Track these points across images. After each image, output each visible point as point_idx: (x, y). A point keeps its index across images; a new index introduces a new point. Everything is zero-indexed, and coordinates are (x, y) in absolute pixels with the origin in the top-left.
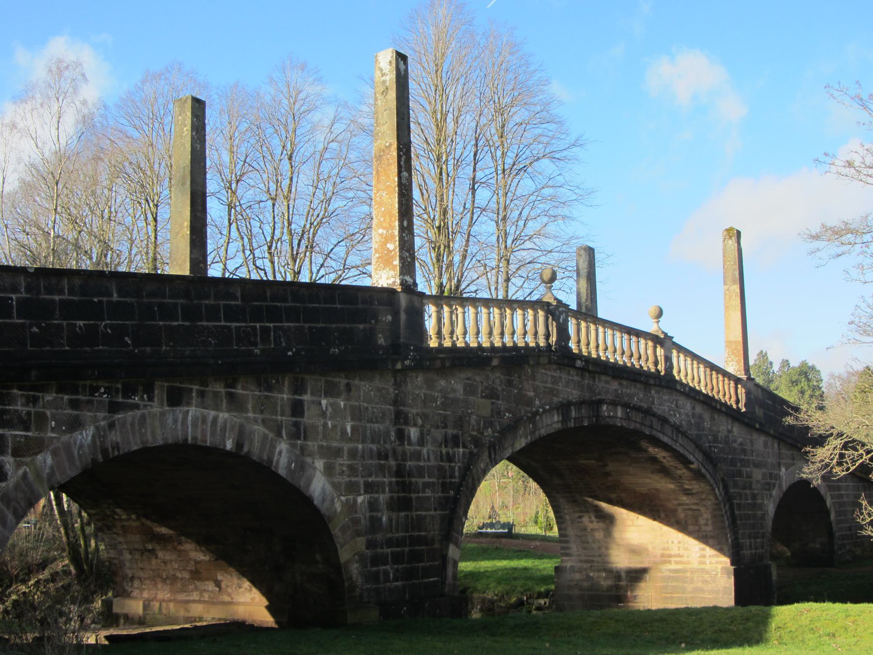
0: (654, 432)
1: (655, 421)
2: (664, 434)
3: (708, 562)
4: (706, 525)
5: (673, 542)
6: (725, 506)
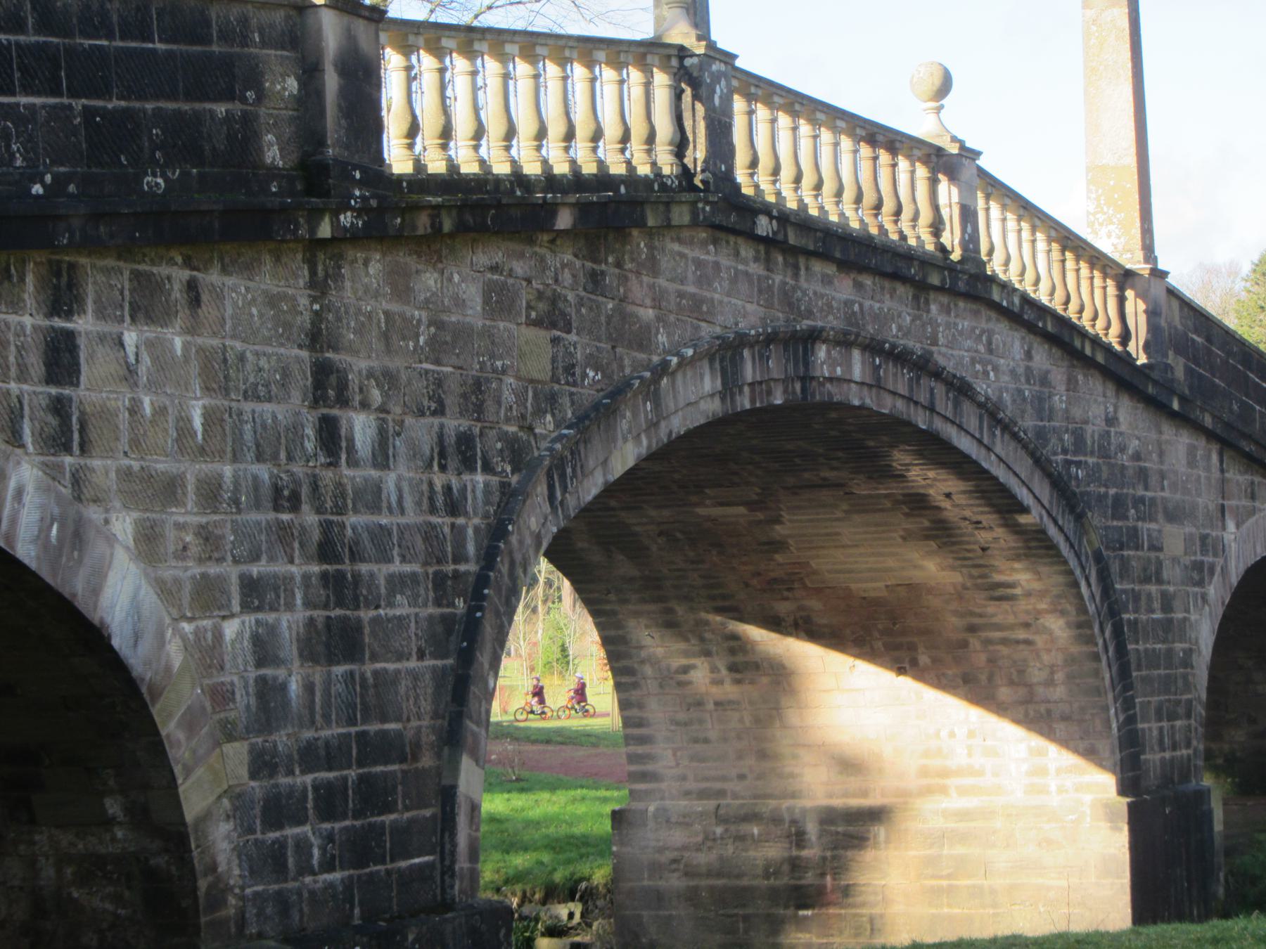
2: (960, 427)
3: (1053, 788)
5: (952, 735)
6: (1102, 631)
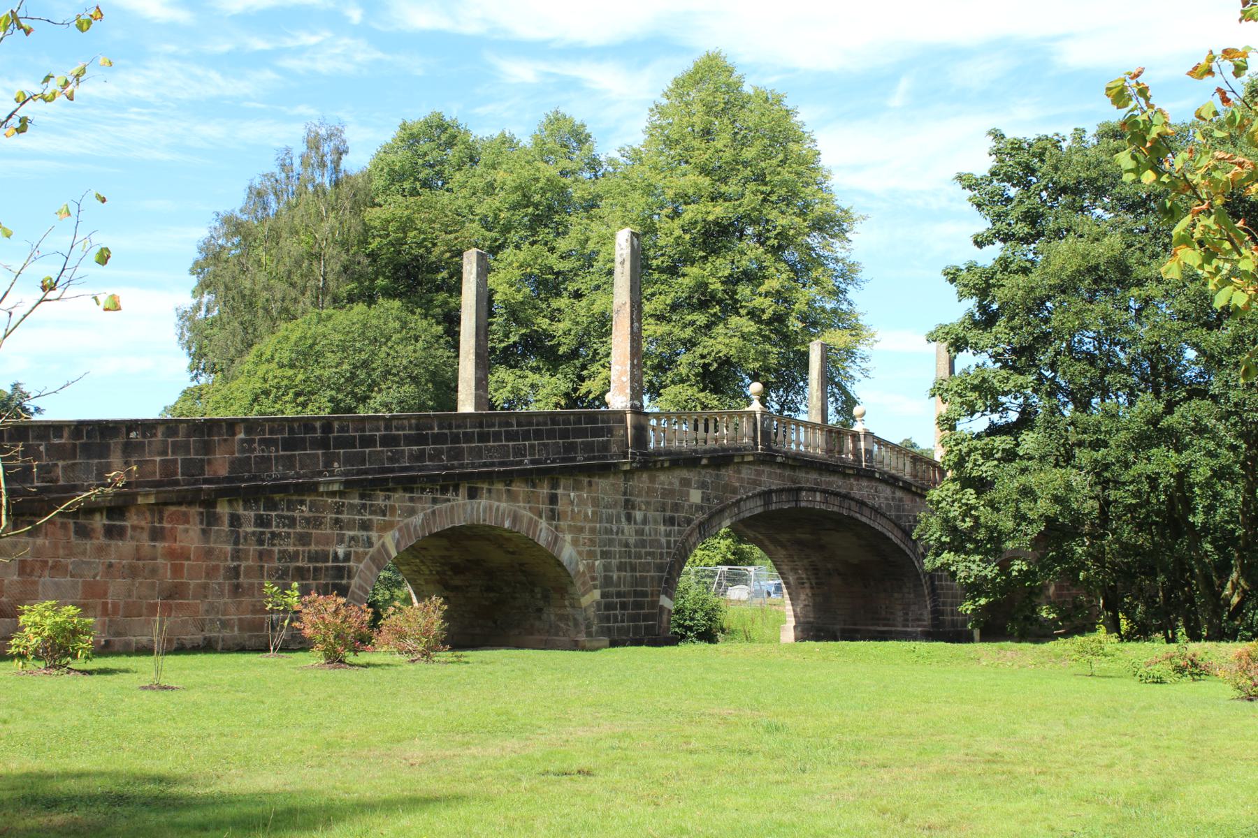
0: (852, 514)
1: (853, 504)
4: (909, 593)
